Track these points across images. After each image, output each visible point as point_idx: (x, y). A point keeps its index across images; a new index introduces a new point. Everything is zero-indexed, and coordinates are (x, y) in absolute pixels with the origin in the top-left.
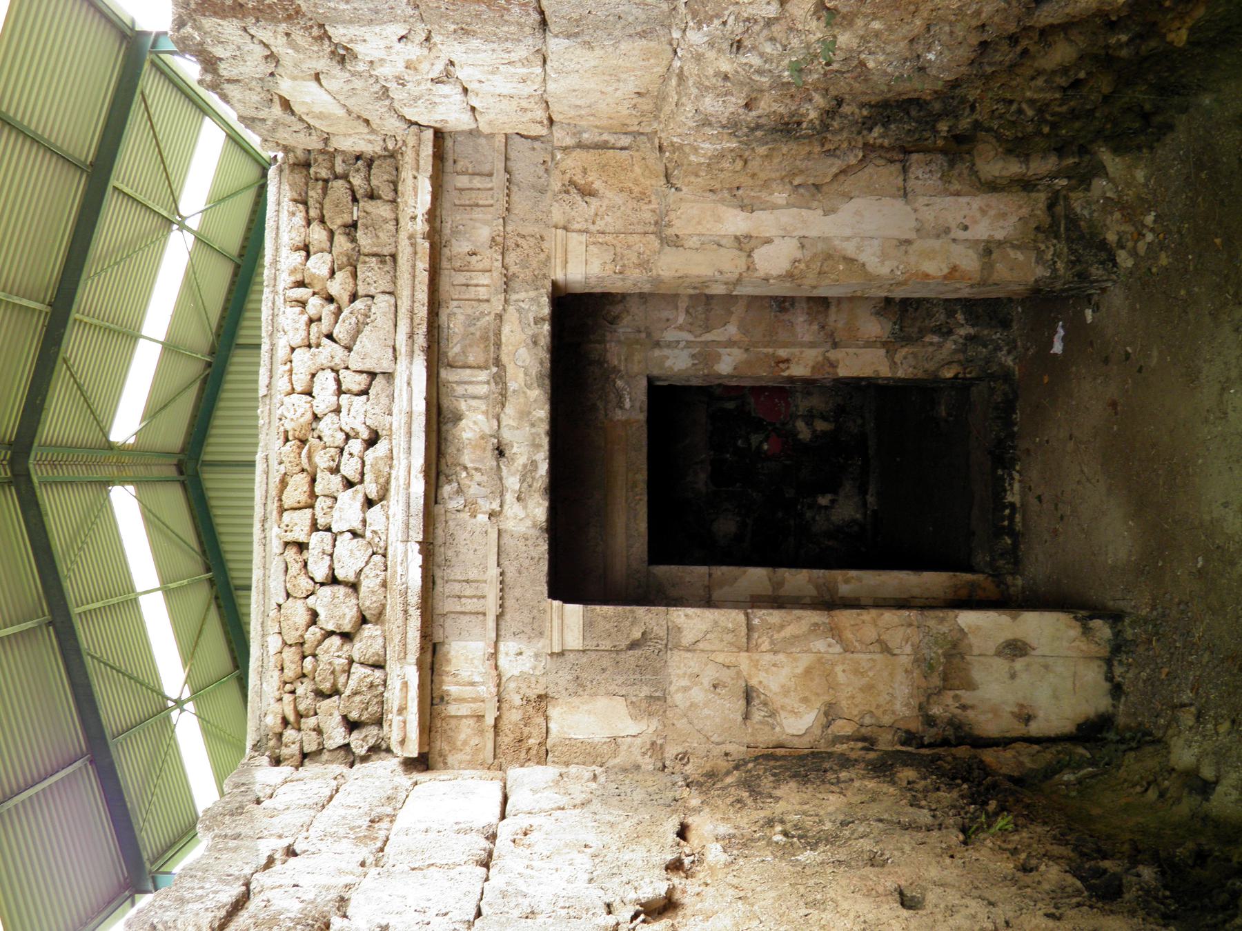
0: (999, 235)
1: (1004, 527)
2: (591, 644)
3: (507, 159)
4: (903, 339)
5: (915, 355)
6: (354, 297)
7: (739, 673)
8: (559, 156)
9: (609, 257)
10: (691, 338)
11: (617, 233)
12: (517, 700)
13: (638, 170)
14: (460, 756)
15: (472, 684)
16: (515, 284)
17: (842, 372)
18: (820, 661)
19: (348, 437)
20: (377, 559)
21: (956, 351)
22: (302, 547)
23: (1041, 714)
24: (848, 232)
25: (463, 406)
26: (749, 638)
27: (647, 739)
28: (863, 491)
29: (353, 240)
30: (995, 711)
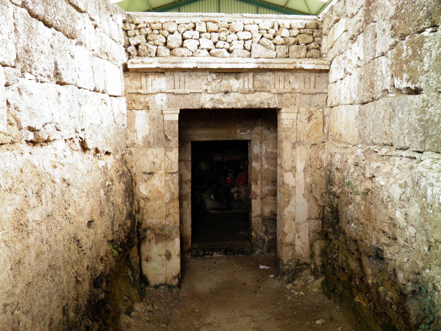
0: (297, 248)
1: (206, 252)
2: (166, 123)
3: (320, 93)
4: (264, 220)
5: (259, 223)
6: (275, 44)
7: (158, 170)
8: (321, 110)
9: (289, 126)
10: (263, 153)
11: (297, 129)
12: (147, 100)
13: (316, 135)
14: (128, 82)
15: (152, 85)
16: (280, 96)
17: (253, 201)
18: (163, 196)
19: (230, 43)
20: (191, 54)
21: (260, 236)
22: (194, 29)
23: (148, 264)
24: (297, 201)
25: (241, 80)
26: (169, 173)
27: (136, 142)
28: (215, 209)
29: (293, 44)
30: (149, 250)
